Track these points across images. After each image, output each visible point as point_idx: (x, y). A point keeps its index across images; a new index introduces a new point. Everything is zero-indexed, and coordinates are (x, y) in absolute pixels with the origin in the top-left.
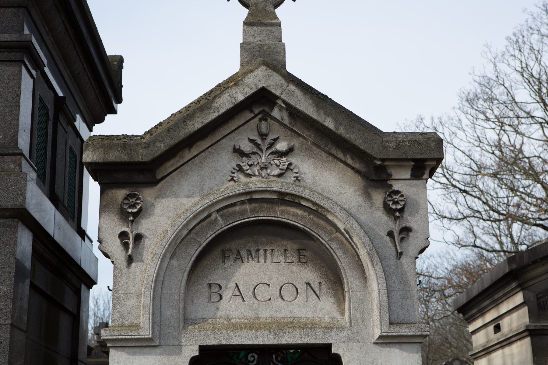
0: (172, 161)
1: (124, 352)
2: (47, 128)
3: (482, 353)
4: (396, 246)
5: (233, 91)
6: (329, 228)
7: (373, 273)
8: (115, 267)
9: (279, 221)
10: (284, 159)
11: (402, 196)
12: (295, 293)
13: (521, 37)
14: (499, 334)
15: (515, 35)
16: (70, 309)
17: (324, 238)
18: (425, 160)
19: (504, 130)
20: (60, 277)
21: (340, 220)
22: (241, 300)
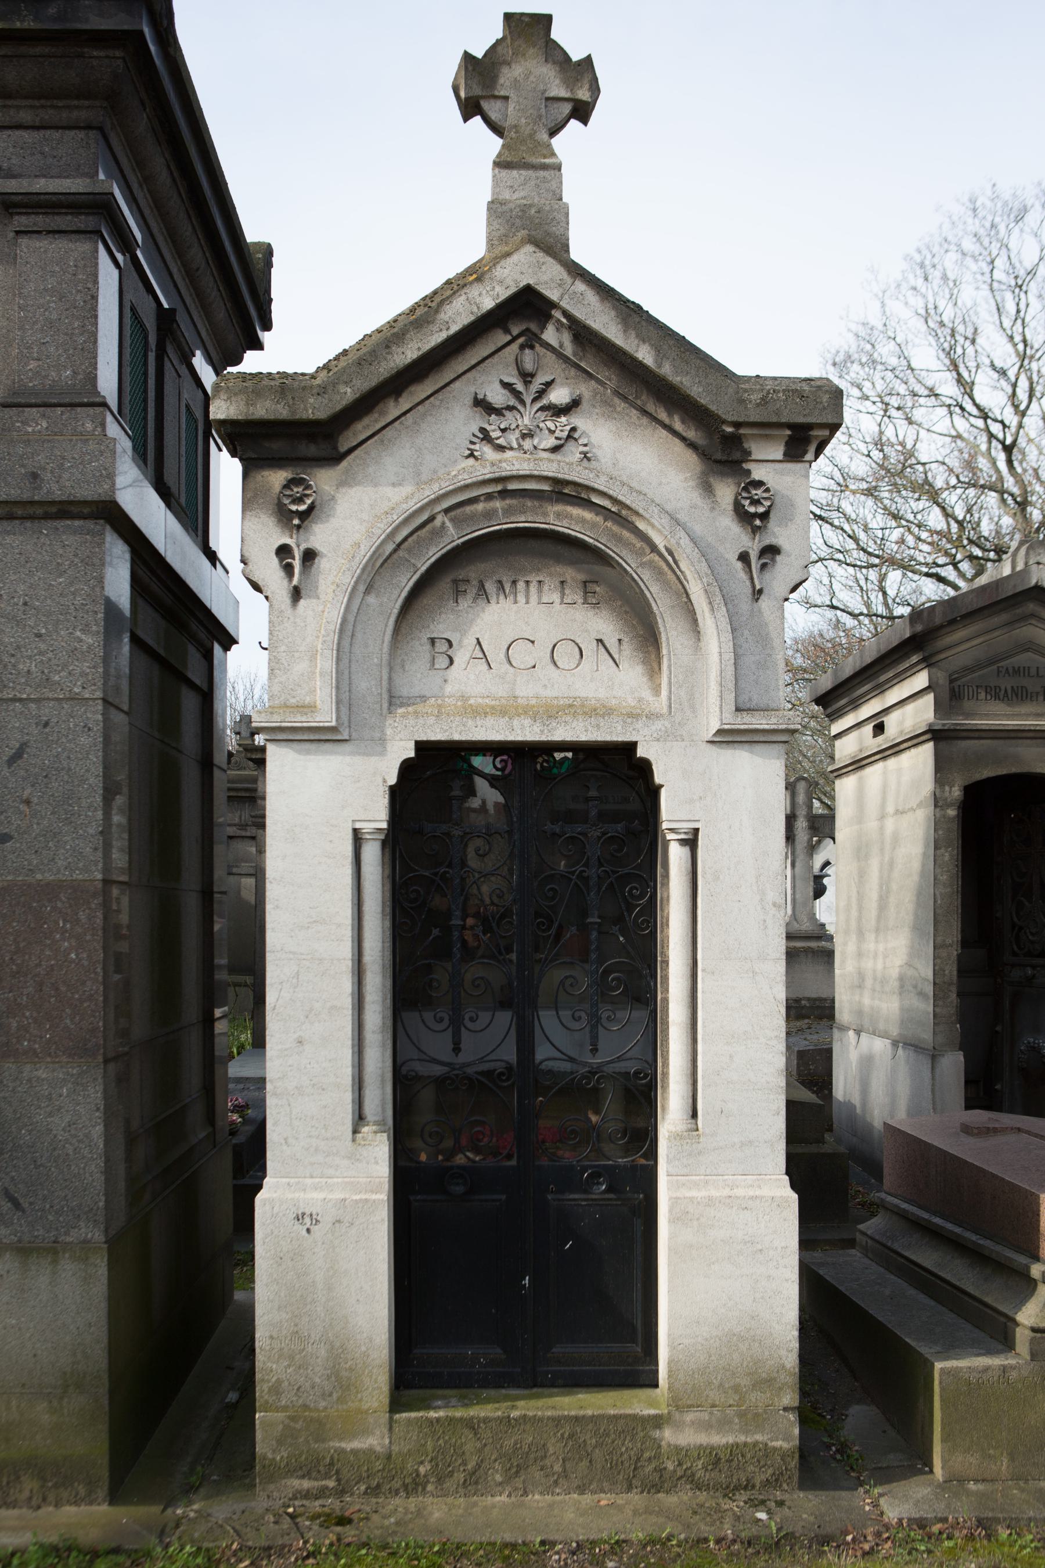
0: (366, 421)
1: (292, 748)
2: (146, 364)
3: (850, 768)
4: (752, 579)
5: (474, 291)
6: (638, 545)
7: (712, 625)
8: (271, 606)
9: (553, 532)
10: (563, 419)
11: (767, 490)
12: (578, 656)
13: (929, 256)
14: (880, 738)
15: (919, 252)
16: (198, 682)
17: (630, 562)
18: (810, 427)
19: (889, 417)
20: (178, 631)
21: (659, 531)
22: (486, 667)
